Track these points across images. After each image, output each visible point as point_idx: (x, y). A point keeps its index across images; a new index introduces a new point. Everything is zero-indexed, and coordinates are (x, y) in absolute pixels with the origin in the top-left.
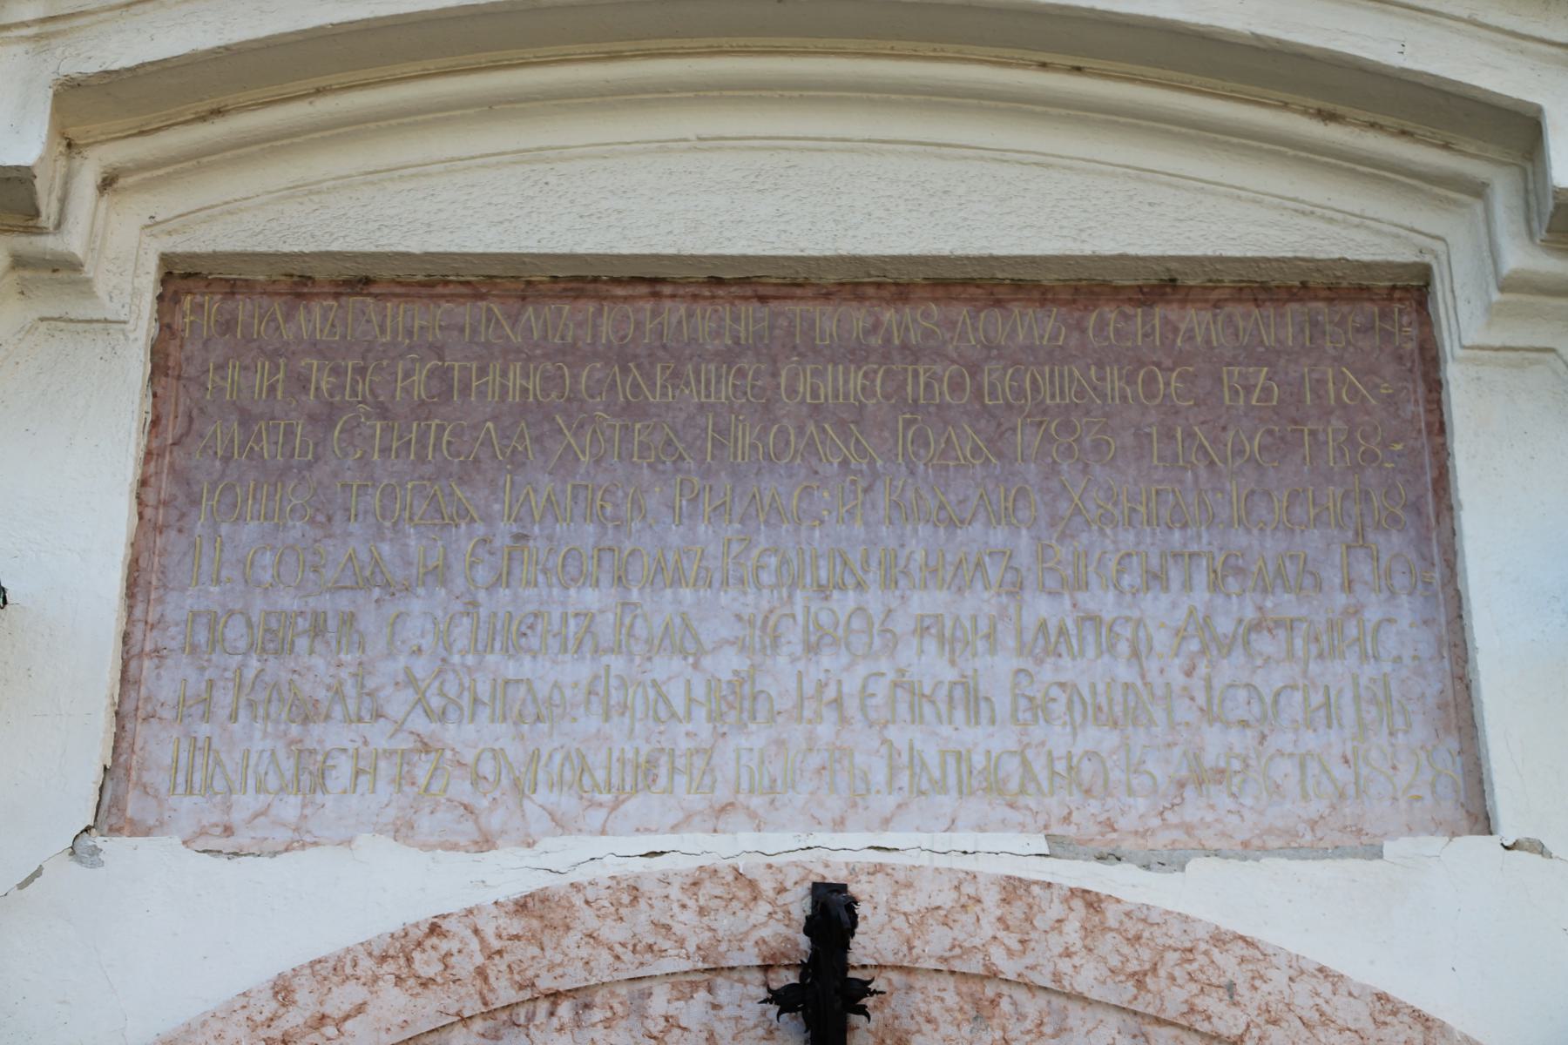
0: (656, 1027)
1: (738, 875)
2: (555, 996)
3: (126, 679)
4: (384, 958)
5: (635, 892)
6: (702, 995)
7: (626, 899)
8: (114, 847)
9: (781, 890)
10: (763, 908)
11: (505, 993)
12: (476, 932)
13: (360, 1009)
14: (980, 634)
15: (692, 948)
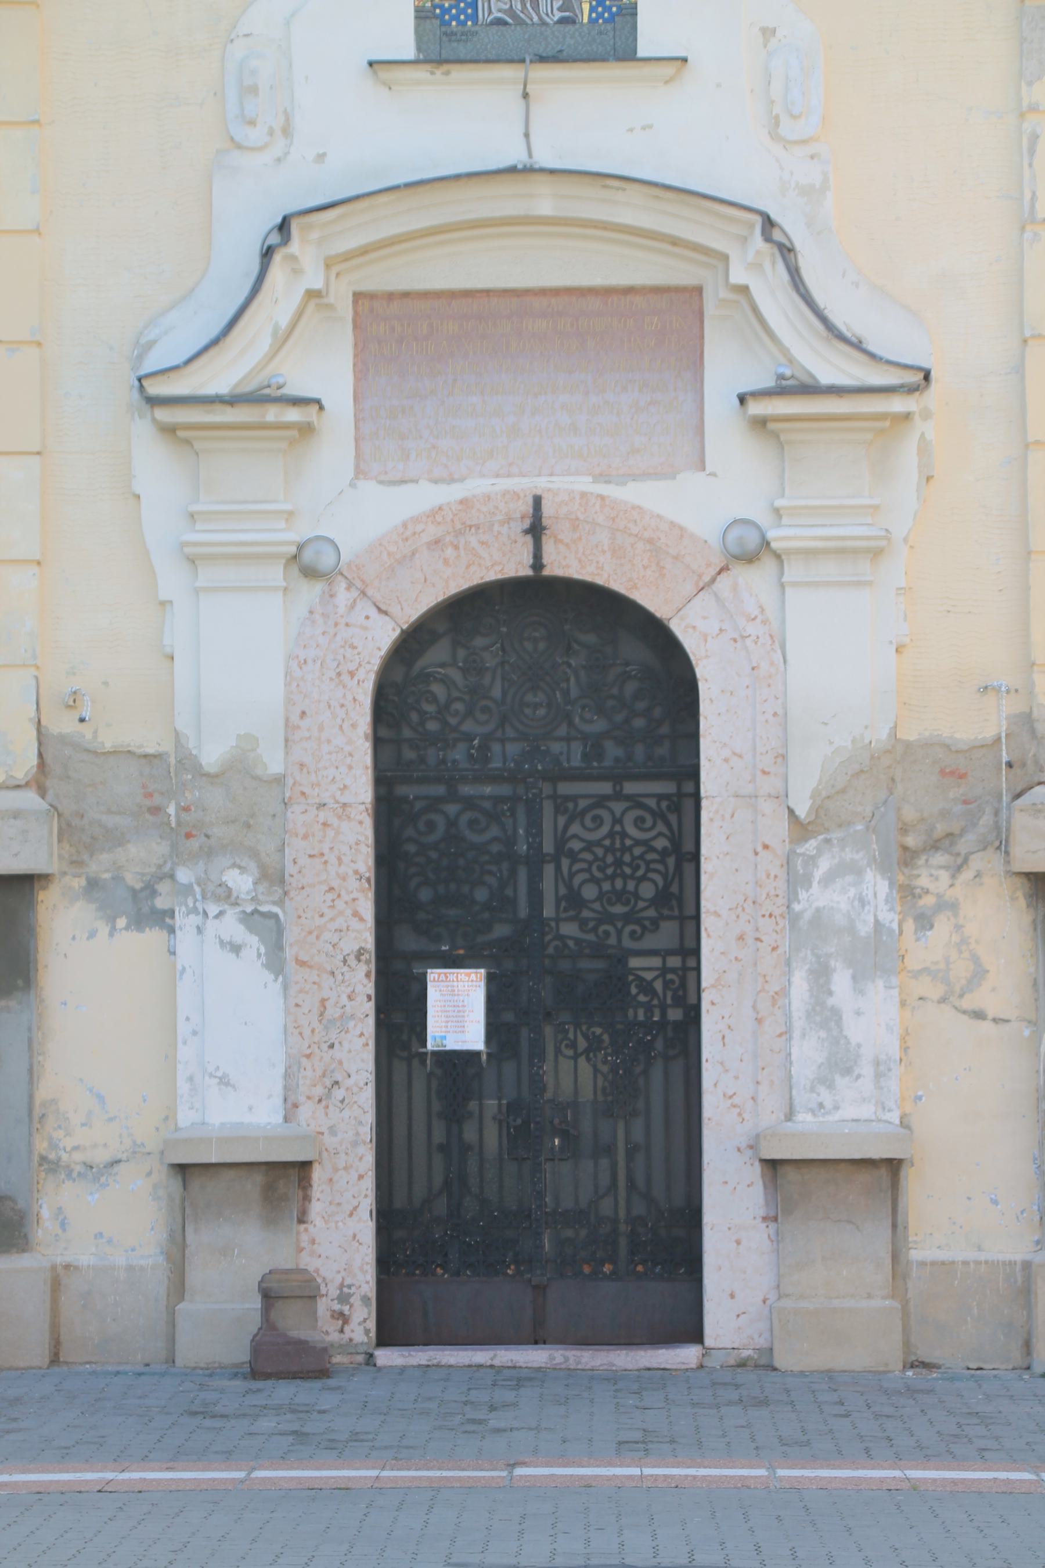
0: (496, 534)
1: (514, 492)
2: (470, 527)
3: (357, 428)
4: (428, 517)
5: (489, 498)
6: (506, 525)
7: (487, 499)
8: (361, 484)
9: (525, 496)
10: (521, 502)
11: (458, 526)
12: (450, 509)
13: (423, 531)
14: (365, 1325)
15: (503, 513)
